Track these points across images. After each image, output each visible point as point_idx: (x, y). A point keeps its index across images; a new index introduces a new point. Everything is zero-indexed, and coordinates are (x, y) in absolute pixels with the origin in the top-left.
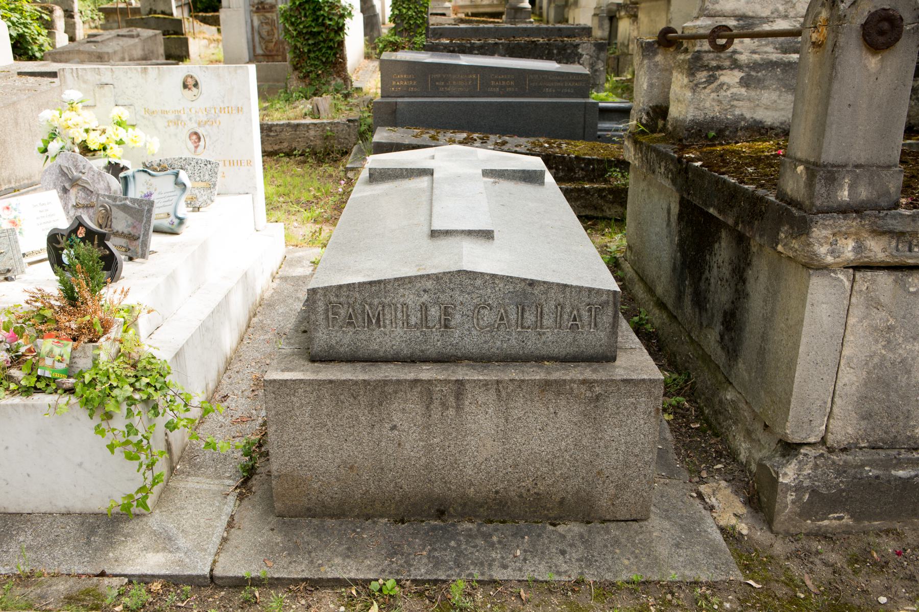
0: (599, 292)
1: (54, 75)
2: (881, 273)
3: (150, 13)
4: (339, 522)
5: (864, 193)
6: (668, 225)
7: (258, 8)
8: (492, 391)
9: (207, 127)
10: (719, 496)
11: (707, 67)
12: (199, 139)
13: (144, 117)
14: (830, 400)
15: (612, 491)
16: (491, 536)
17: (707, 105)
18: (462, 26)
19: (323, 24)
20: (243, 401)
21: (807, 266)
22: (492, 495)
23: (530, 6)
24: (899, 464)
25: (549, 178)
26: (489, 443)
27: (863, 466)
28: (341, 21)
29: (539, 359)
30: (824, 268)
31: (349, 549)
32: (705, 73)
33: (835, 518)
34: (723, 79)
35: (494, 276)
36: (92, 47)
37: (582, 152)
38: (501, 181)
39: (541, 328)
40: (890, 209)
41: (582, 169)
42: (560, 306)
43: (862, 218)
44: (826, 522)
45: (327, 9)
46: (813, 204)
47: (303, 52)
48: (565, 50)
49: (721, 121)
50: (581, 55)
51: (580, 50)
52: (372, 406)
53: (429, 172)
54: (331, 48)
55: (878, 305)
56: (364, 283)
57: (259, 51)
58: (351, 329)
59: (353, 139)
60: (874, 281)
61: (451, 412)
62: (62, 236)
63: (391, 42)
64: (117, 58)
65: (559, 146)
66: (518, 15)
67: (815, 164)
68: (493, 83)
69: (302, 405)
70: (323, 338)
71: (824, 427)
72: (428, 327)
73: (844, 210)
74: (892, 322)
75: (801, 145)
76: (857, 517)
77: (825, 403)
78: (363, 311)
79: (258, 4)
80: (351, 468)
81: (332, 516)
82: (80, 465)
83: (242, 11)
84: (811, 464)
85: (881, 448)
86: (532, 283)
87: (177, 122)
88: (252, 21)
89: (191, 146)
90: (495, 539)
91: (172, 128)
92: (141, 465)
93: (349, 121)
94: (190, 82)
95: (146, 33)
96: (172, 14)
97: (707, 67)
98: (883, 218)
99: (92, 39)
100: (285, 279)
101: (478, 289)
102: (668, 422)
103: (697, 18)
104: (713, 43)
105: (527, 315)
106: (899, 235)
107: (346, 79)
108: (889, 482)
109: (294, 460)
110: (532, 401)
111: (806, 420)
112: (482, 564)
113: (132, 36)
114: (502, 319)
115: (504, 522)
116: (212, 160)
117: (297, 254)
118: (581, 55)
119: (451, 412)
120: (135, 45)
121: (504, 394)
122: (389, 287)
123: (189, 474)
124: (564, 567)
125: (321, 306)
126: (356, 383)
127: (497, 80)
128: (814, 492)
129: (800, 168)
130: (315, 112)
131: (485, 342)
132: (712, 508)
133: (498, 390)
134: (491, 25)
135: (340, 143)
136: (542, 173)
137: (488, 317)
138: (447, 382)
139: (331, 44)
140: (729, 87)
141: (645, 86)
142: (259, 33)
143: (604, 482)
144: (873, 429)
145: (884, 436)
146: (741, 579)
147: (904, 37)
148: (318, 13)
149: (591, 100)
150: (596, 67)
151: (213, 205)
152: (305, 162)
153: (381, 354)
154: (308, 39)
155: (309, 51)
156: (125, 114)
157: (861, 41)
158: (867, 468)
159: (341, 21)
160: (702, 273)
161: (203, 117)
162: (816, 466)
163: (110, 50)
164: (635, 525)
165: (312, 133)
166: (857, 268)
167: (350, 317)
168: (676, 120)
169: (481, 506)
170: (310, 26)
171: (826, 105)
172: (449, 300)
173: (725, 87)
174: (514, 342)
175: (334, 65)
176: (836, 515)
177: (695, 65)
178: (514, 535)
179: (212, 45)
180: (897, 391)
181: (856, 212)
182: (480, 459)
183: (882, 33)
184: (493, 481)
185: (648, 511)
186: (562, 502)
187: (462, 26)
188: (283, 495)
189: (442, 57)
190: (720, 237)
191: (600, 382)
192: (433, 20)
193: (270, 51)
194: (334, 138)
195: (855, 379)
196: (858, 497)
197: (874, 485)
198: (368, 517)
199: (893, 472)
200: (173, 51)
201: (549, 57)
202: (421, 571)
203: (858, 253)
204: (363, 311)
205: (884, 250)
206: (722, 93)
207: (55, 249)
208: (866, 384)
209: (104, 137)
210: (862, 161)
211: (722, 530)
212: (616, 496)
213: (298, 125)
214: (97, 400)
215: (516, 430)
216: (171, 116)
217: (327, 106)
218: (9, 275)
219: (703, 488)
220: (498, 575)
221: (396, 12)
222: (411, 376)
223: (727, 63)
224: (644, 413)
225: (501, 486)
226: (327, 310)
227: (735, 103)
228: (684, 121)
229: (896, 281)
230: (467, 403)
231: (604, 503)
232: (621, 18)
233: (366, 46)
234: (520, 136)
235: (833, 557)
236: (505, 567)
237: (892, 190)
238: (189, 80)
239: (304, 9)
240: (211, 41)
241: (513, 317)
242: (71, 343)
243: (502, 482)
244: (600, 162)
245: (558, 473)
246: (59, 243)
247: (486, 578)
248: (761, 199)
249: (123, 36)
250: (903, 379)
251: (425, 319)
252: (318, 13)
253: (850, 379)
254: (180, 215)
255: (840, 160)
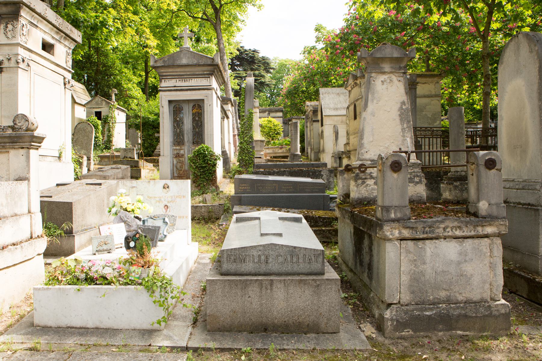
0: (317, 250)
1: (100, 184)
2: (409, 241)
3: (124, 158)
4: (229, 333)
5: (399, 215)
6: (351, 238)
7: (176, 156)
8: (283, 283)
9: (171, 203)
10: (366, 327)
11: (361, 178)
12: (168, 207)
13: (147, 199)
14: (399, 287)
15: (326, 321)
16: (283, 337)
17: (363, 192)
18: (269, 163)
19: (207, 163)
20: (190, 301)
21: (385, 240)
22: (283, 323)
23: (300, 154)
24: (426, 310)
25: (304, 221)
26: (282, 303)
27: (413, 311)
28: (215, 161)
29: (299, 274)
30: (390, 240)
31: (234, 340)
32: (361, 181)
33: (407, 332)
34: (368, 182)
35: (282, 245)
36: (101, 173)
37: (321, 215)
38: (286, 221)
39: (299, 263)
40: (408, 220)
41: (321, 222)
42: (305, 255)
43: (399, 223)
44: (403, 333)
45: (209, 157)
46: (383, 219)
47: (198, 175)
48: (315, 173)
49: (368, 198)
50: (323, 175)
51: (322, 173)
52: (242, 289)
53: (259, 219)
54: (210, 173)
55: (410, 252)
56: (240, 248)
57: (176, 175)
58: (235, 264)
59: (221, 212)
60: (407, 244)
61: (269, 291)
62: (131, 237)
63: (238, 171)
64: (112, 178)
65: (312, 213)
66: (295, 157)
67: (383, 206)
68: (283, 187)
69: (219, 289)
70: (226, 267)
71: (399, 297)
72: (261, 263)
73: (393, 221)
74: (415, 258)
75: (380, 202)
76: (415, 331)
77: (397, 288)
78: (239, 257)
79: (176, 154)
80: (234, 312)
81: (227, 331)
82: (141, 311)
83: (169, 157)
84: (395, 310)
85: (419, 304)
86: (295, 248)
87: (160, 201)
88: (173, 162)
89: (164, 210)
90: (285, 338)
91: (158, 204)
92: (164, 308)
93: (219, 204)
94: (166, 186)
95: (124, 167)
96: (134, 158)
97: (361, 178)
98: (406, 223)
99: (101, 170)
100: (199, 263)
101: (277, 249)
102: (351, 308)
103: (357, 161)
104: (360, 170)
105: (294, 258)
106: (412, 228)
107: (217, 187)
108: (423, 316)
109: (215, 309)
110: (296, 287)
111: (392, 294)
112: (280, 344)
113: (118, 168)
114: (285, 260)
115: (288, 333)
116: (175, 215)
117: (203, 256)
118: (323, 175)
119: (269, 291)
120: (119, 172)
121: (286, 284)
122: (248, 249)
123: (174, 321)
124: (309, 345)
125: (225, 256)
126: (237, 280)
127: (285, 186)
128: (397, 321)
129: (380, 208)
130: (205, 201)
131: (280, 268)
132: (364, 331)
133: (284, 283)
134: (282, 163)
135: (215, 214)
136: (301, 218)
137: (281, 259)
138: (267, 280)
139: (211, 171)
140: (370, 186)
141: (341, 186)
142: (176, 167)
143: (322, 318)
144: (415, 297)
145: (420, 300)
146: (371, 348)
147: (403, 168)
148: (205, 158)
149: (326, 194)
150: (330, 180)
151: (174, 232)
152: (199, 223)
153: (245, 272)
154: (200, 169)
155: (201, 175)
156: (141, 198)
157: (391, 170)
158: (415, 312)
159: (215, 161)
160: (361, 252)
161: (170, 199)
162: (397, 311)
163: (109, 175)
164: (335, 334)
165: (203, 210)
166: (401, 240)
167: (235, 260)
168: (352, 198)
169: (280, 327)
170: (202, 164)
171: (384, 188)
172: (267, 253)
173: (369, 186)
174: (289, 268)
175: (212, 180)
176: (407, 330)
177: (357, 178)
178: (292, 337)
179: (151, 172)
180: (421, 283)
181: (397, 221)
182: (279, 309)
183: (396, 167)
184: (284, 317)
185: (339, 329)
186: (308, 325)
187: (269, 163)
188: (210, 323)
189: (261, 177)
190: (365, 238)
191: (319, 280)
192: (256, 161)
193: (181, 175)
194: (213, 212)
195: (406, 279)
196: (414, 323)
197: (418, 318)
198: (240, 331)
199: (424, 313)
200: (134, 175)
201: (308, 176)
202: (259, 346)
203: (400, 235)
204: (239, 257)
205: (408, 233)
206: (368, 188)
207: (127, 241)
208: (410, 280)
209: (133, 206)
210: (397, 205)
211: (367, 337)
212: (327, 323)
213: (197, 206)
214: (150, 287)
215: (291, 297)
216: (158, 199)
217: (210, 198)
218: (110, 251)
219: (361, 326)
220: (286, 347)
221: (240, 158)
222: (256, 278)
223: (369, 177)
224: (335, 291)
225: (286, 319)
226: (227, 257)
227: (373, 191)
228: (355, 198)
229: (414, 244)
230: (274, 288)
231: (323, 326)
232: (343, 158)
233: (224, 172)
234: (295, 209)
235: (406, 344)
236: (288, 345)
237: (408, 214)
238: (166, 185)
239: (199, 157)
240: (150, 170)
241: (289, 259)
242: (141, 268)
243: (287, 317)
244: (329, 218)
245: (306, 314)
246: (129, 239)
247: (282, 348)
248: (372, 220)
249: (114, 168)
250: (423, 278)
251: (260, 260)
252: (205, 158)
253: (405, 278)
254: (165, 234)
255: (390, 205)
